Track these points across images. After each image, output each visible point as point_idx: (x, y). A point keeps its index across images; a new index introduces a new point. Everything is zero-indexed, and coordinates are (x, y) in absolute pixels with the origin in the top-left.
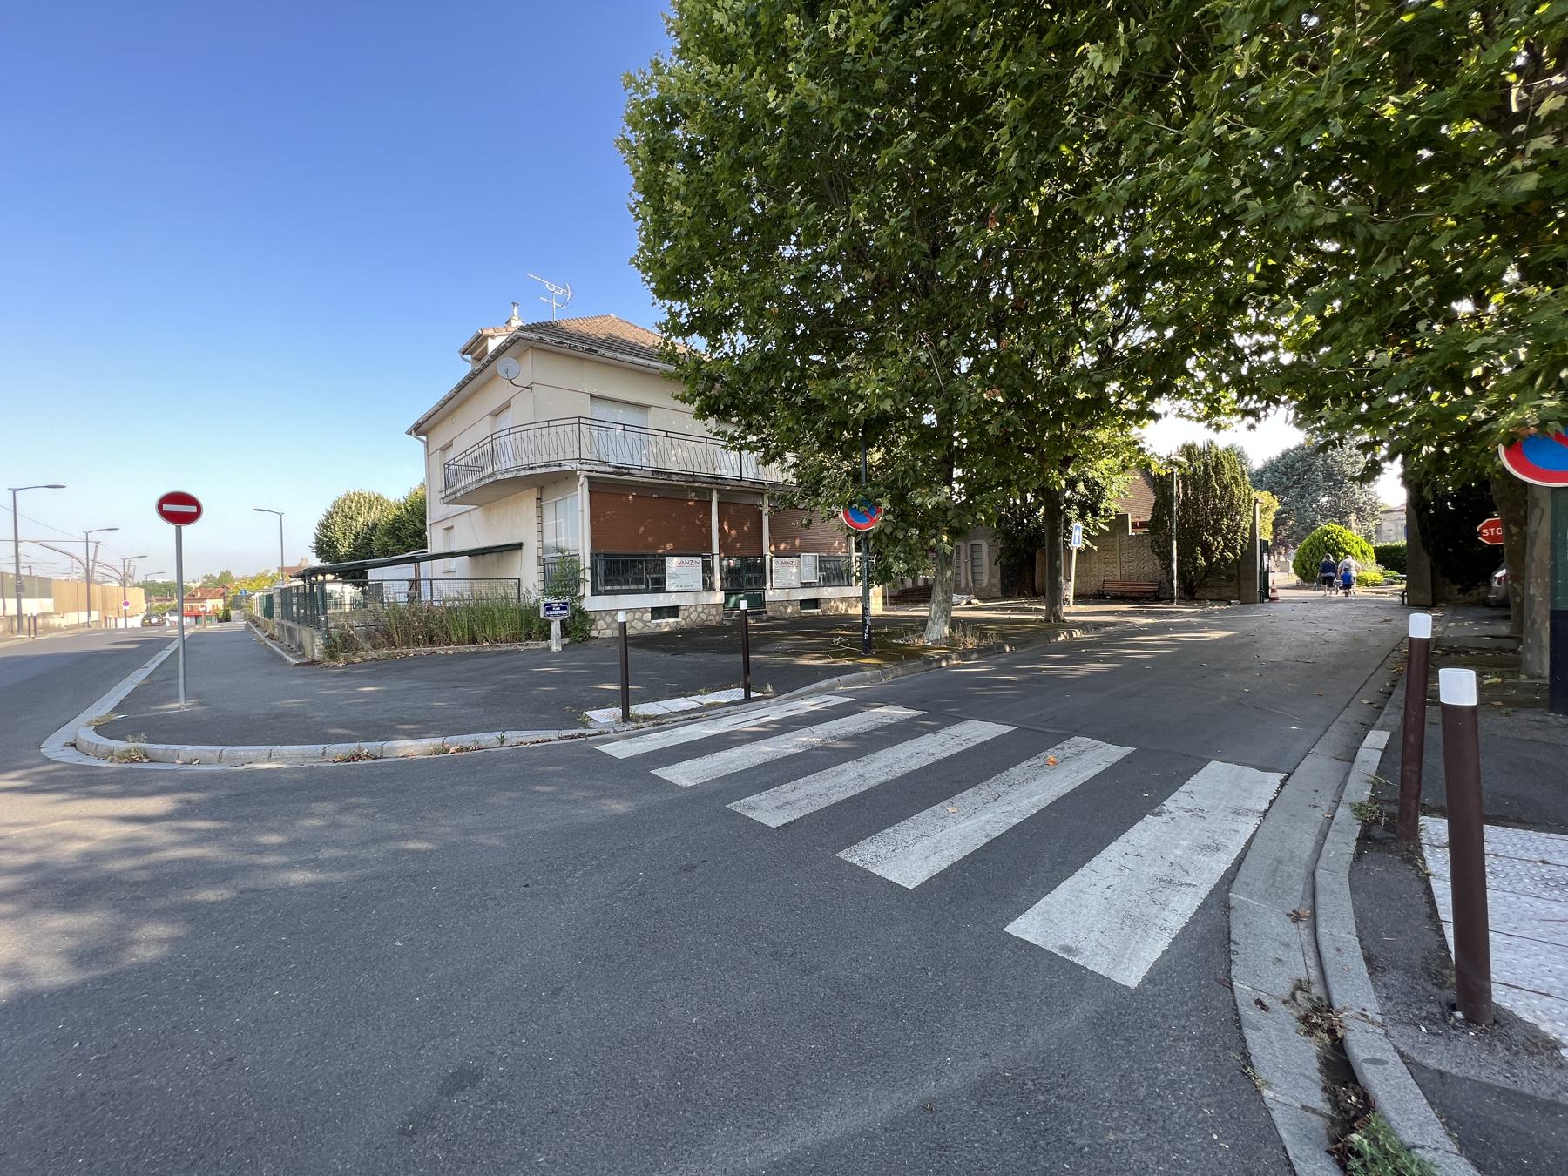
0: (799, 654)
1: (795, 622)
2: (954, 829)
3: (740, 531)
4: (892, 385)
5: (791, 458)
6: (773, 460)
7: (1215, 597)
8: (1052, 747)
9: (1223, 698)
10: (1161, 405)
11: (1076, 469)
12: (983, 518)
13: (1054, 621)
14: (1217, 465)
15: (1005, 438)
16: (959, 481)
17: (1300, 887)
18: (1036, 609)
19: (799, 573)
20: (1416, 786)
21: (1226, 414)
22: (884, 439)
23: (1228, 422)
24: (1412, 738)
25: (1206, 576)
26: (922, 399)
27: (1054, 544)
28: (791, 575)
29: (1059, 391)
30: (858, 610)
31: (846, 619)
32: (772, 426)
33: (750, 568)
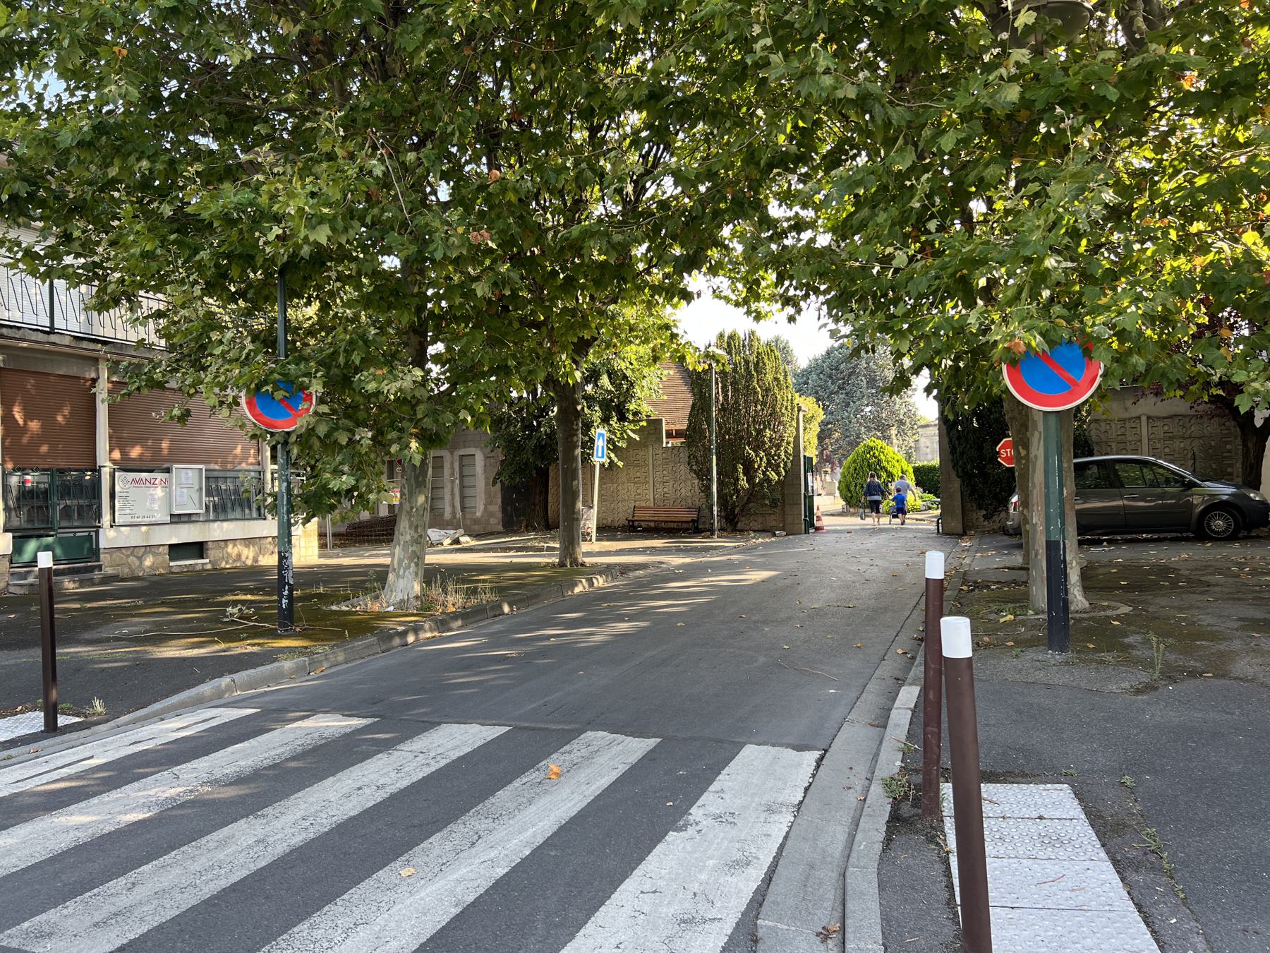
0: (160, 639)
1: (157, 583)
2: (408, 902)
3: (48, 423)
4: (330, 206)
5: (151, 302)
6: (116, 302)
7: (759, 527)
8: (556, 751)
9: (762, 659)
10: (695, 281)
11: (598, 354)
12: (469, 419)
13: (570, 566)
14: (758, 362)
15: (502, 306)
16: (437, 359)
17: (830, 895)
18: (549, 549)
19: (169, 497)
20: (936, 749)
21: (766, 300)
22: (319, 288)
23: (767, 309)
24: (931, 696)
25: (749, 501)
26: (377, 234)
27: (570, 458)
28: (153, 501)
29: (571, 247)
30: (270, 560)
31: (255, 572)
32: (113, 244)
33: (66, 491)
